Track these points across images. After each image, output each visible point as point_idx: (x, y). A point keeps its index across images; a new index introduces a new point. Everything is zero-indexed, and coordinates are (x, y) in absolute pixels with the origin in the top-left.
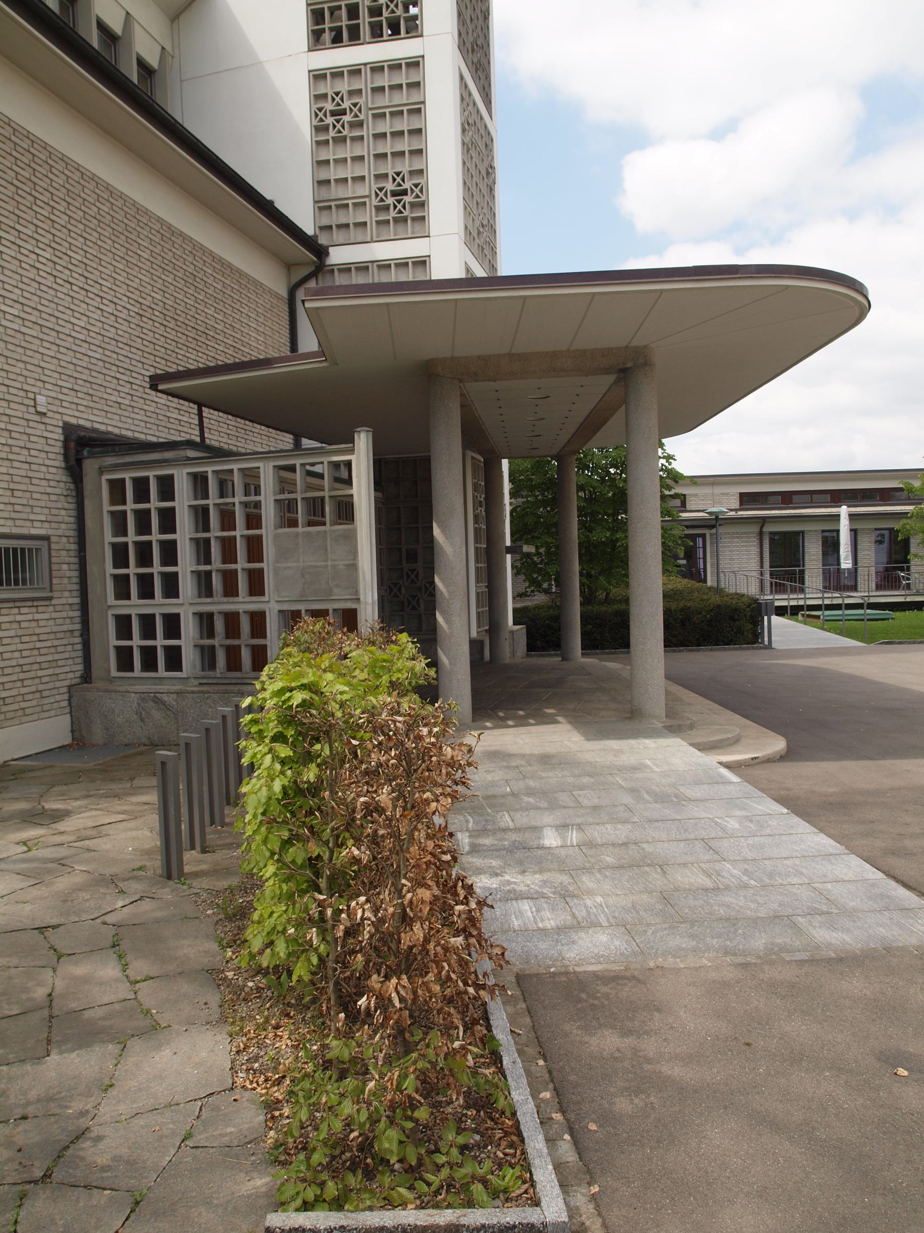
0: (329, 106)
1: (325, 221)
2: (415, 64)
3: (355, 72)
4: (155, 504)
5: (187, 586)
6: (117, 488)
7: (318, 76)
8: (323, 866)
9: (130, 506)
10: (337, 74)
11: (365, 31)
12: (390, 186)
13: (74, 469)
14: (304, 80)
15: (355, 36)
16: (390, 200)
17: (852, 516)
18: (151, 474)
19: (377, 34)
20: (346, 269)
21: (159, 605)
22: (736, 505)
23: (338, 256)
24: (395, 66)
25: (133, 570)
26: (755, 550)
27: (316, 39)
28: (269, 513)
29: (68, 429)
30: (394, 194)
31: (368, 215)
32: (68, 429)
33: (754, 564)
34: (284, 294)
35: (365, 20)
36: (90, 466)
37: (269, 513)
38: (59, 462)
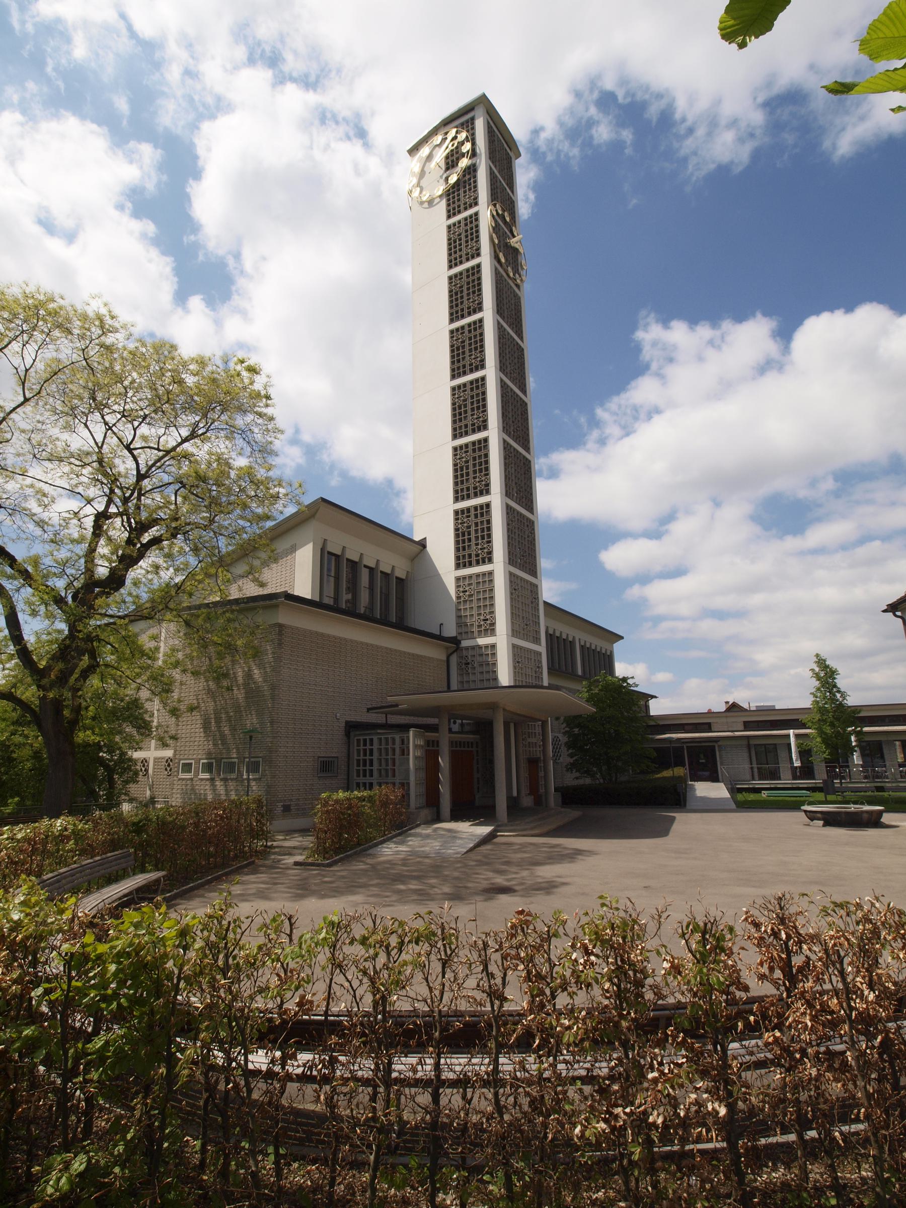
0: (461, 589)
1: (460, 631)
2: (491, 573)
3: (470, 577)
4: (368, 747)
5: (375, 773)
6: (358, 741)
7: (458, 579)
8: (116, 696)
9: (362, 747)
10: (464, 578)
11: (474, 562)
12: (482, 618)
13: (348, 734)
14: (453, 581)
15: (470, 565)
16: (482, 623)
17: (797, 736)
18: (367, 737)
19: (478, 563)
20: (467, 648)
21: (368, 780)
22: (742, 728)
23: (465, 643)
24: (484, 574)
25: (361, 768)
26: (746, 755)
27: (458, 566)
28: (398, 751)
29: (347, 723)
30: (484, 620)
31: (475, 629)
32: (347, 723)
33: (747, 766)
34: (445, 659)
35: (474, 558)
36: (352, 734)
37: (398, 751)
38: (343, 733)
